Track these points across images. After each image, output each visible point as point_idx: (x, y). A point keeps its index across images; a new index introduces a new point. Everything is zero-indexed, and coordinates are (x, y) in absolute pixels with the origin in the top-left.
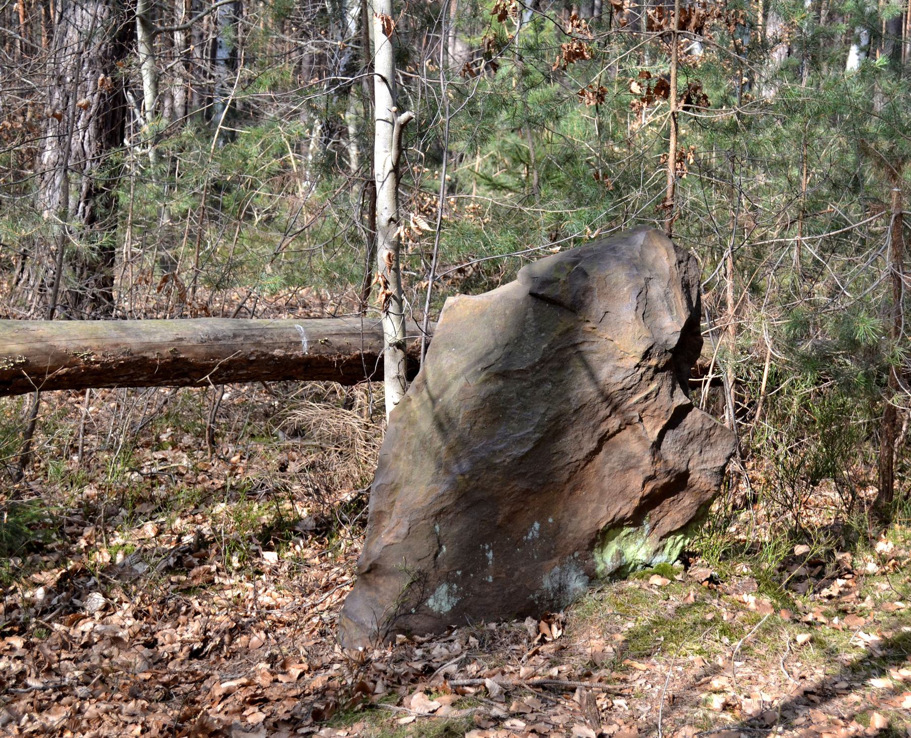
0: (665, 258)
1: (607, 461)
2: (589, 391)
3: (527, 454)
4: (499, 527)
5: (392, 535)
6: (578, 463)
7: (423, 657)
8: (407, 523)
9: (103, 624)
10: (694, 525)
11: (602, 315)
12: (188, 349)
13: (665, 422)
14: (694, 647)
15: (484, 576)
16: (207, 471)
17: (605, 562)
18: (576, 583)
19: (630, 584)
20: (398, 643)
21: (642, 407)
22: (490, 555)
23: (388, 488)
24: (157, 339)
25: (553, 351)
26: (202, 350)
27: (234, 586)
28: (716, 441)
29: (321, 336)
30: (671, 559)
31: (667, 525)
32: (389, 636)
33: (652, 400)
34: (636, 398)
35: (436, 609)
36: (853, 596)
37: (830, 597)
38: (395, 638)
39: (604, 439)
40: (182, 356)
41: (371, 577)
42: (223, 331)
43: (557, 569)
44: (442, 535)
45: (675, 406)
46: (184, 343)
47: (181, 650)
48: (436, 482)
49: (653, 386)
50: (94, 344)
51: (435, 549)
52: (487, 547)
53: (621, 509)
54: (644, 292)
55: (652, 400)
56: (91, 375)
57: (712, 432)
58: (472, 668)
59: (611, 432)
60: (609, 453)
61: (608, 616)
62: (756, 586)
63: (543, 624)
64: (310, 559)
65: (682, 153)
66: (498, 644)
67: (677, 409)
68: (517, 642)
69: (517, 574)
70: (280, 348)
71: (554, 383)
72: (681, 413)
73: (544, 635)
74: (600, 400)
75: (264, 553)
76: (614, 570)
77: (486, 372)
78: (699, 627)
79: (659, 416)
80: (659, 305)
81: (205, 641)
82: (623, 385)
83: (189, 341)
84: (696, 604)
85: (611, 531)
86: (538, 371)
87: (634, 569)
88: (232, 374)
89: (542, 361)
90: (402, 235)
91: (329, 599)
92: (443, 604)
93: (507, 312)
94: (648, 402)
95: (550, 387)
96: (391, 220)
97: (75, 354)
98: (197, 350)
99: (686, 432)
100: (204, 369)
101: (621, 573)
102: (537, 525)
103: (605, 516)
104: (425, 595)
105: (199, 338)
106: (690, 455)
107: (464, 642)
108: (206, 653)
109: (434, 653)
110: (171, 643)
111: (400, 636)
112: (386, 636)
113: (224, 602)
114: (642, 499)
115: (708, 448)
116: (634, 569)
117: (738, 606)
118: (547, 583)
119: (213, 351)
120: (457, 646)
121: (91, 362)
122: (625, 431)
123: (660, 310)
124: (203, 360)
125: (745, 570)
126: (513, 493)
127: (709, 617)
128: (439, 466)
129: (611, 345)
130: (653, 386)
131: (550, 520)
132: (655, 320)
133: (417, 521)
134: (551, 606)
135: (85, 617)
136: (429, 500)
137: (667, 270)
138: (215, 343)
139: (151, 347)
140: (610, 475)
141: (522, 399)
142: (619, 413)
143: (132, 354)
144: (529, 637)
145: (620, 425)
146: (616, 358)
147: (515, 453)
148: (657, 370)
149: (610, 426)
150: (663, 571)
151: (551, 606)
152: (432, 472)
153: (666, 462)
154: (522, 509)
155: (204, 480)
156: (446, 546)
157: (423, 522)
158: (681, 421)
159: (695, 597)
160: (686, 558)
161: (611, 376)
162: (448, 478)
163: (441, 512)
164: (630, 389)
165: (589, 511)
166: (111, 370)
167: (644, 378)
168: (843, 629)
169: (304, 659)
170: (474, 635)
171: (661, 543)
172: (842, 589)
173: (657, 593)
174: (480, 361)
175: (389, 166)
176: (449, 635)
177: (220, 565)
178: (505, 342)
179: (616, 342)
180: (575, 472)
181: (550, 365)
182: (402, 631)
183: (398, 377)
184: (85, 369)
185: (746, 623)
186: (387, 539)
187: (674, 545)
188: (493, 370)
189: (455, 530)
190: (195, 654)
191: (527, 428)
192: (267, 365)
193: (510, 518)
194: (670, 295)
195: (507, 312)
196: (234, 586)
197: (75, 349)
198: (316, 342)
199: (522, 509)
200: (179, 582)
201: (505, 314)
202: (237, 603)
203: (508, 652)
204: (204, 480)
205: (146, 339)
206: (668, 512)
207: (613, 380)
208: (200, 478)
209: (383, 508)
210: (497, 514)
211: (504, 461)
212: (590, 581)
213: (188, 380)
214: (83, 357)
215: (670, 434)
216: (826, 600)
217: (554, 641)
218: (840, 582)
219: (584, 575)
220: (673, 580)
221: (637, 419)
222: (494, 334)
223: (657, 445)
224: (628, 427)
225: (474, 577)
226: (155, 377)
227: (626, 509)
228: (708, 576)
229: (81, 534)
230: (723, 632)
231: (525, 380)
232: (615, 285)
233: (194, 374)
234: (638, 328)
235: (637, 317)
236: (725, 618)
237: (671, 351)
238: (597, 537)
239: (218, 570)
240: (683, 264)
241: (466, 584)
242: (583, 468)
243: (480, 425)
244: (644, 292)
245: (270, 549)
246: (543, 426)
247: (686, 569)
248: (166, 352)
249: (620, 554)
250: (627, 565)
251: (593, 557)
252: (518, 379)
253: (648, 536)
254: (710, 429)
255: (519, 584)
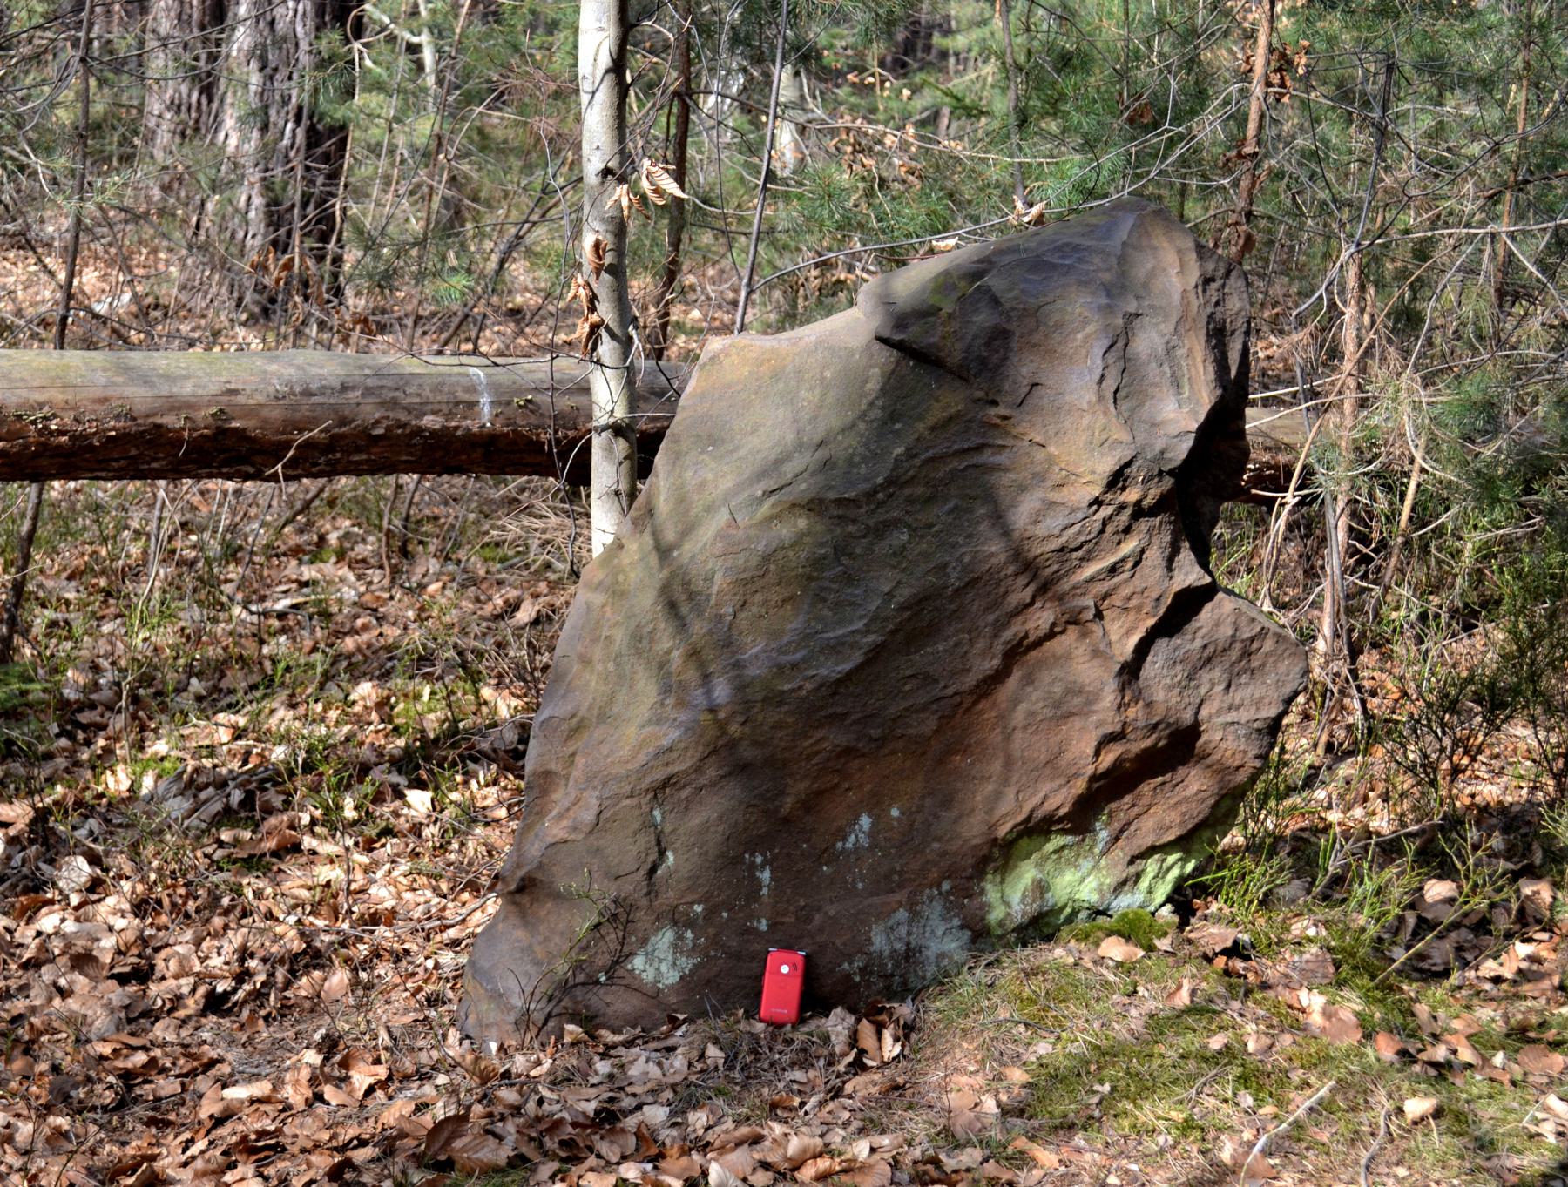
0: (1173, 271)
1: (1024, 700)
2: (995, 549)
3: (849, 676)
4: (786, 820)
5: (565, 823)
6: (958, 699)
7: (611, 1077)
8: (594, 802)
9: (77, 920)
10: (1206, 834)
11: (1026, 390)
12: (249, 411)
13: (1151, 622)
14: (1173, 1114)
15: (750, 917)
16: (375, 610)
17: (1007, 904)
18: (943, 941)
19: (1059, 952)
20: (567, 1039)
21: (1103, 587)
22: (766, 876)
23: (565, 726)
24: (186, 390)
25: (917, 462)
26: (276, 414)
27: (329, 863)
28: (1263, 665)
29: (520, 391)
30: (1151, 901)
31: (1147, 831)
32: (551, 1024)
33: (1126, 575)
34: (1090, 570)
35: (648, 977)
36: (1546, 984)
37: (1497, 980)
38: (562, 1029)
39: (1016, 652)
40: (234, 424)
41: (525, 899)
42: (322, 377)
43: (902, 914)
44: (668, 829)
45: (1176, 588)
46: (241, 399)
47: (193, 991)
48: (659, 722)
49: (1130, 546)
50: (58, 396)
51: (651, 858)
52: (759, 859)
53: (1045, 798)
54: (1120, 344)
55: (1126, 575)
56: (52, 457)
57: (1255, 645)
58: (698, 1119)
59: (1032, 638)
60: (1029, 680)
61: (999, 1025)
62: (1331, 969)
63: (866, 1028)
64: (493, 808)
65: (1283, 56)
66: (766, 1066)
67: (1178, 595)
68: (804, 1063)
69: (818, 917)
70: (434, 413)
71: (913, 530)
72: (1188, 604)
73: (862, 1052)
74: (1011, 569)
75: (407, 792)
76: (1025, 920)
77: (774, 498)
78: (1192, 1065)
79: (1139, 608)
80: (1152, 371)
81: (242, 976)
82: (1063, 540)
83: (250, 396)
84: (1193, 1010)
85: (1024, 842)
86: (881, 504)
87: (1070, 920)
88: (338, 461)
89: (890, 482)
90: (625, 203)
91: (478, 914)
92: (664, 968)
93: (828, 374)
94: (1117, 579)
95: (905, 537)
96: (607, 172)
97: (19, 417)
98: (265, 413)
99: (1198, 644)
100: (275, 451)
101: (1042, 926)
102: (865, 821)
103: (1009, 813)
104: (626, 949)
105: (271, 390)
106: (1203, 691)
107: (695, 1054)
108: (235, 1004)
109: (634, 1071)
110: (177, 977)
111: (570, 1027)
112: (534, 1028)
113: (305, 894)
114: (1094, 778)
115: (1244, 679)
116: (1070, 920)
117: (1291, 1020)
118: (879, 941)
119: (298, 416)
120: (678, 1062)
121: (51, 433)
122: (1063, 637)
123: (1155, 385)
124: (278, 432)
125: (1312, 932)
126: (817, 753)
127: (1216, 1043)
128: (666, 690)
129: (1040, 455)
130: (1130, 546)
131: (895, 813)
132: (1141, 405)
133: (617, 798)
134: (888, 988)
135: (51, 902)
136: (642, 758)
137: (1176, 297)
138: (304, 400)
139: (175, 405)
140: (1025, 728)
141: (845, 560)
142: (1051, 599)
143: (134, 419)
144: (832, 1054)
145: (1054, 624)
146: (1049, 483)
147: (823, 672)
148: (1139, 512)
149: (1030, 625)
150: (1131, 930)
151: (888, 988)
152: (652, 701)
153: (1149, 705)
154: (837, 786)
155: (365, 628)
156: (675, 851)
157: (628, 802)
158: (1187, 621)
159: (1193, 992)
160: (1184, 901)
161: (1036, 522)
162: (683, 716)
163: (666, 783)
164: (1077, 549)
165: (978, 798)
166: (91, 447)
167: (1109, 529)
168: (1514, 1083)
169: (384, 1056)
170: (716, 1041)
171: (1132, 869)
172: (1524, 965)
173: (1111, 977)
174: (762, 474)
175: (605, 61)
176: (668, 1035)
177: (318, 813)
178: (817, 438)
179: (1052, 449)
180: (951, 717)
181: (907, 491)
182: (574, 1018)
183: (617, 493)
184: (38, 444)
185: (1297, 1063)
186: (555, 831)
187: (1161, 875)
188: (788, 495)
189: (696, 819)
190: (215, 1004)
191: (851, 622)
192: (408, 445)
193: (809, 804)
194: (1179, 352)
195: (828, 374)
196: (329, 863)
197: (19, 406)
198: (509, 403)
199: (837, 786)
200: (237, 842)
201: (823, 379)
202: (326, 900)
203: (781, 1085)
204: (365, 628)
205: (165, 390)
206: (1150, 806)
207: (1040, 530)
208: (359, 622)
209: (553, 767)
210: (782, 793)
211: (800, 687)
212: (974, 940)
213: (251, 470)
214: (34, 422)
215: (1162, 647)
216: (1488, 986)
217: (884, 1064)
218: (1522, 949)
219: (962, 927)
220: (1150, 948)
221: (1090, 614)
222: (796, 421)
223: (1131, 671)
224: (1071, 628)
225: (729, 919)
226: (182, 462)
227: (1061, 799)
228: (1229, 944)
229: (104, 727)
230: (1244, 1080)
231: (854, 521)
232: (1059, 326)
233: (258, 459)
234: (1102, 420)
235: (1101, 398)
236: (1251, 1047)
237: (1171, 473)
238: (991, 852)
239: (314, 822)
240: (1214, 286)
241: (712, 931)
242: (968, 709)
243: (755, 610)
244: (1120, 344)
245: (420, 785)
246: (887, 619)
247: (1184, 923)
248: (204, 414)
249: (1041, 888)
250: (1055, 911)
251: (983, 892)
252: (839, 517)
253: (1103, 853)
254: (1252, 639)
255: (820, 939)
